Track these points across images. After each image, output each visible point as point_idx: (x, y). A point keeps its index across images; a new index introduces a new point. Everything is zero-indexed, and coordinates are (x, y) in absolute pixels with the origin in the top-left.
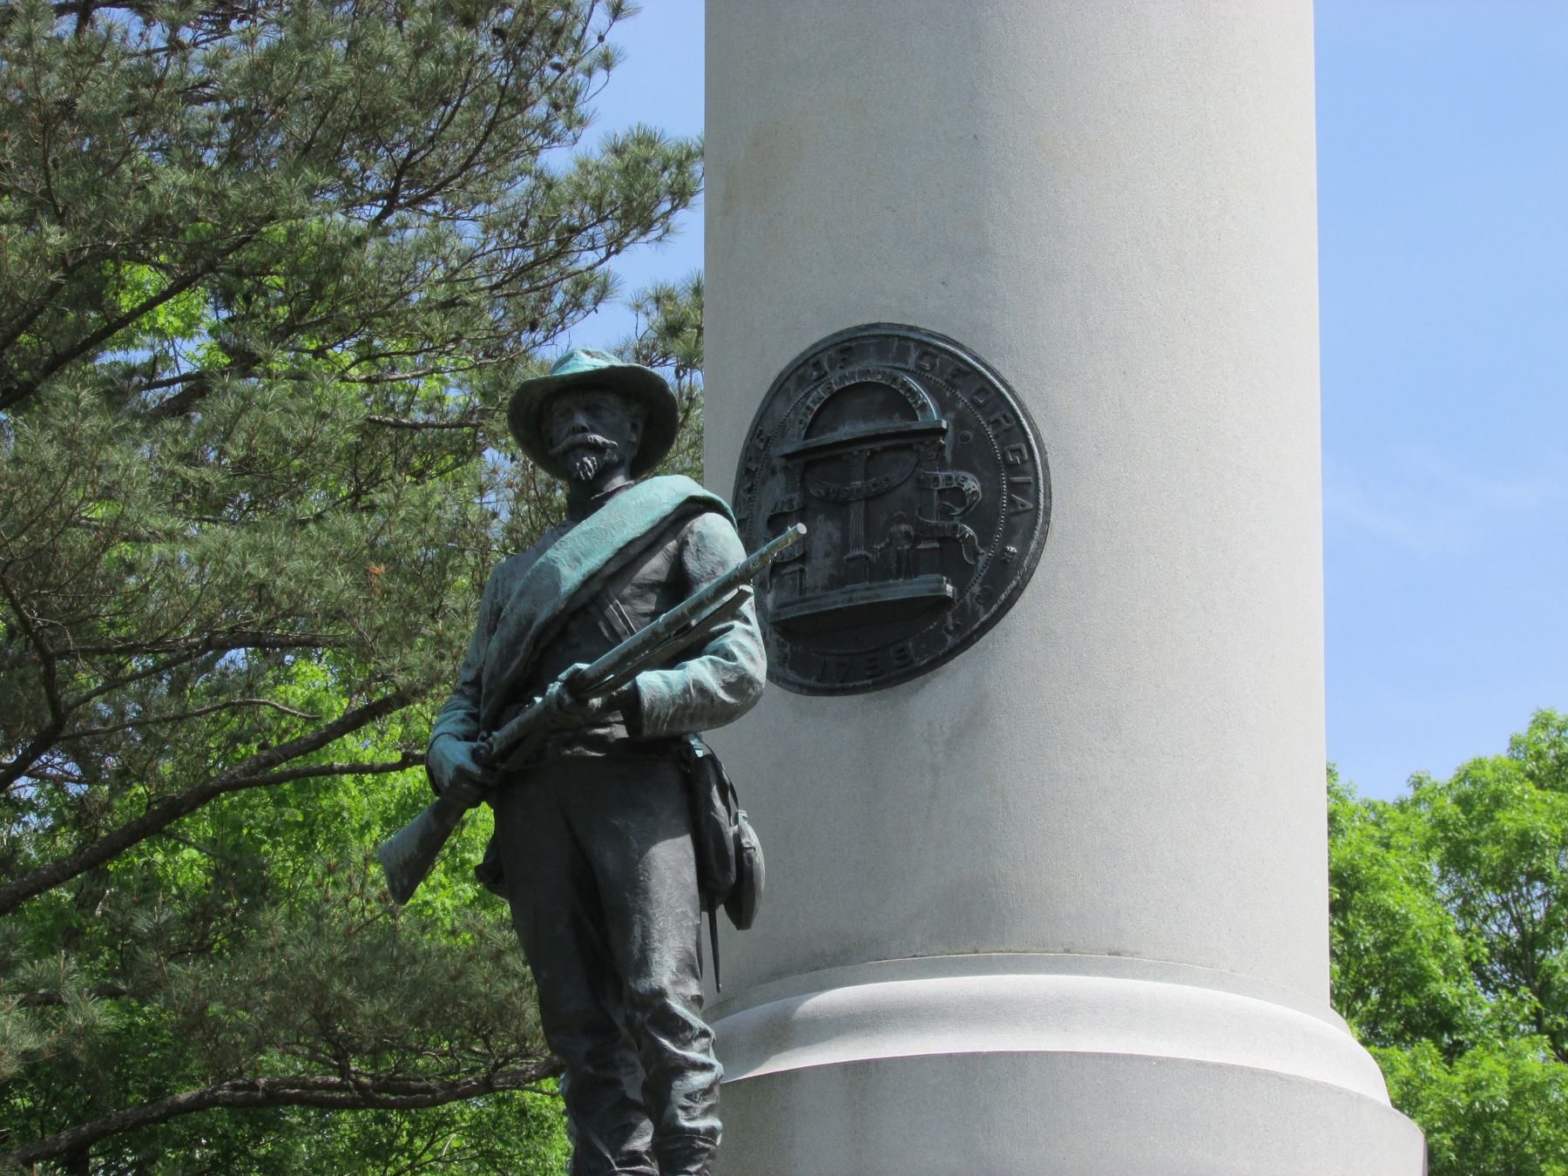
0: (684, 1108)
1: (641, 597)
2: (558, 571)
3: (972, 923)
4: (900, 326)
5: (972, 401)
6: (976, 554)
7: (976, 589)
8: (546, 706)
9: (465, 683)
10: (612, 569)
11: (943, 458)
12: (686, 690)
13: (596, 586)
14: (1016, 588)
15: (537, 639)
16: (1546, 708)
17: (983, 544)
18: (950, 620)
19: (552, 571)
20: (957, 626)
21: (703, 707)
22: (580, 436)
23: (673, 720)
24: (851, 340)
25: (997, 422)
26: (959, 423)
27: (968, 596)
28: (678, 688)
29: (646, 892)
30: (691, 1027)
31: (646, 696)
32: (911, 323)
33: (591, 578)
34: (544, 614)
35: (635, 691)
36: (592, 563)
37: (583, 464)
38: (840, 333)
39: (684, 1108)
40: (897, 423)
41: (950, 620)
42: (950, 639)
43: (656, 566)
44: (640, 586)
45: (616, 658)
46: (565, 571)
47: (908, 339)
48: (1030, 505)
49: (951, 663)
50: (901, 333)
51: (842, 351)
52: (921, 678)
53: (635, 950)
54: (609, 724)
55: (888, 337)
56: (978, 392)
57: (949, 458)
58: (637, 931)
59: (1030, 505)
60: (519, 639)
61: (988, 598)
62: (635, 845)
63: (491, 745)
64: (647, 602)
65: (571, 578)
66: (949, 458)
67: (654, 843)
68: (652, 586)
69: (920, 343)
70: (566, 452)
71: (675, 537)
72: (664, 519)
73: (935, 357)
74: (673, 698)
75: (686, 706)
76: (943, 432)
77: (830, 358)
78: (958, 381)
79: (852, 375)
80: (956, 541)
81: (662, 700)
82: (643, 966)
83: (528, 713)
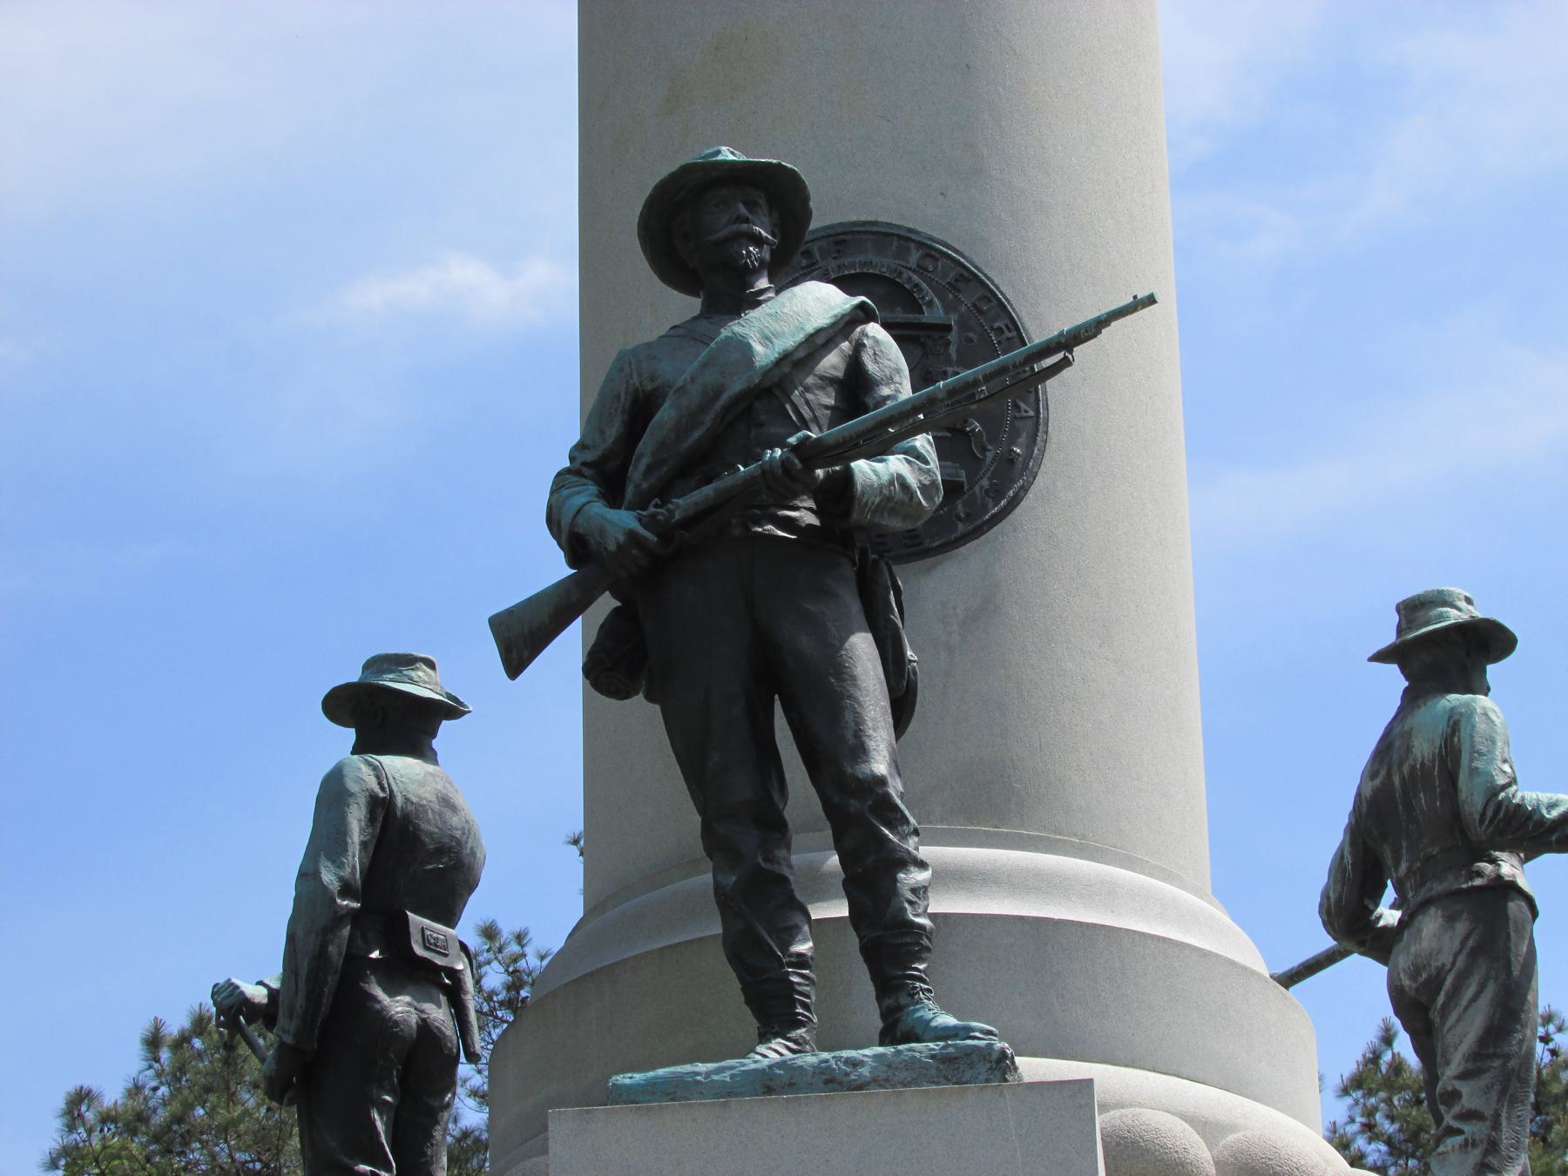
0: (911, 903)
1: (822, 388)
2: (750, 346)
3: (997, 801)
4: (900, 227)
5: (974, 305)
6: (984, 450)
7: (985, 483)
8: (750, 481)
9: (584, 464)
10: (801, 354)
11: (949, 356)
12: (891, 483)
13: (786, 369)
14: (1021, 488)
15: (728, 408)
16: (87, 1083)
17: (991, 441)
18: (960, 507)
19: (744, 348)
20: (968, 515)
21: (903, 503)
22: (745, 226)
23: (878, 510)
24: (845, 233)
25: (1000, 329)
26: (964, 324)
27: (977, 488)
28: (885, 478)
29: (854, 678)
30: (907, 822)
31: (859, 479)
32: (911, 226)
33: (786, 357)
34: (737, 386)
35: (848, 476)
36: (788, 342)
37: (749, 252)
38: (832, 227)
39: (911, 903)
40: (911, 317)
41: (960, 507)
42: (960, 526)
43: (833, 362)
44: (822, 378)
45: (871, 424)
46: (758, 348)
47: (909, 239)
48: (1031, 413)
49: (962, 549)
50: (902, 233)
51: (837, 243)
52: (929, 561)
53: (849, 736)
54: (796, 509)
55: (885, 234)
56: (980, 299)
57: (954, 355)
58: (849, 717)
59: (1031, 413)
60: (705, 405)
61: (996, 492)
62: (834, 631)
63: (671, 512)
64: (828, 395)
65: (764, 354)
66: (954, 355)
67: (853, 633)
68: (832, 381)
69: (921, 245)
70: (727, 240)
71: (846, 338)
72: (843, 316)
73: (937, 260)
74: (881, 487)
75: (889, 499)
76: (948, 328)
77: (820, 249)
78: (961, 285)
79: (853, 266)
80: (967, 434)
81: (871, 486)
82: (860, 751)
83: (726, 481)
